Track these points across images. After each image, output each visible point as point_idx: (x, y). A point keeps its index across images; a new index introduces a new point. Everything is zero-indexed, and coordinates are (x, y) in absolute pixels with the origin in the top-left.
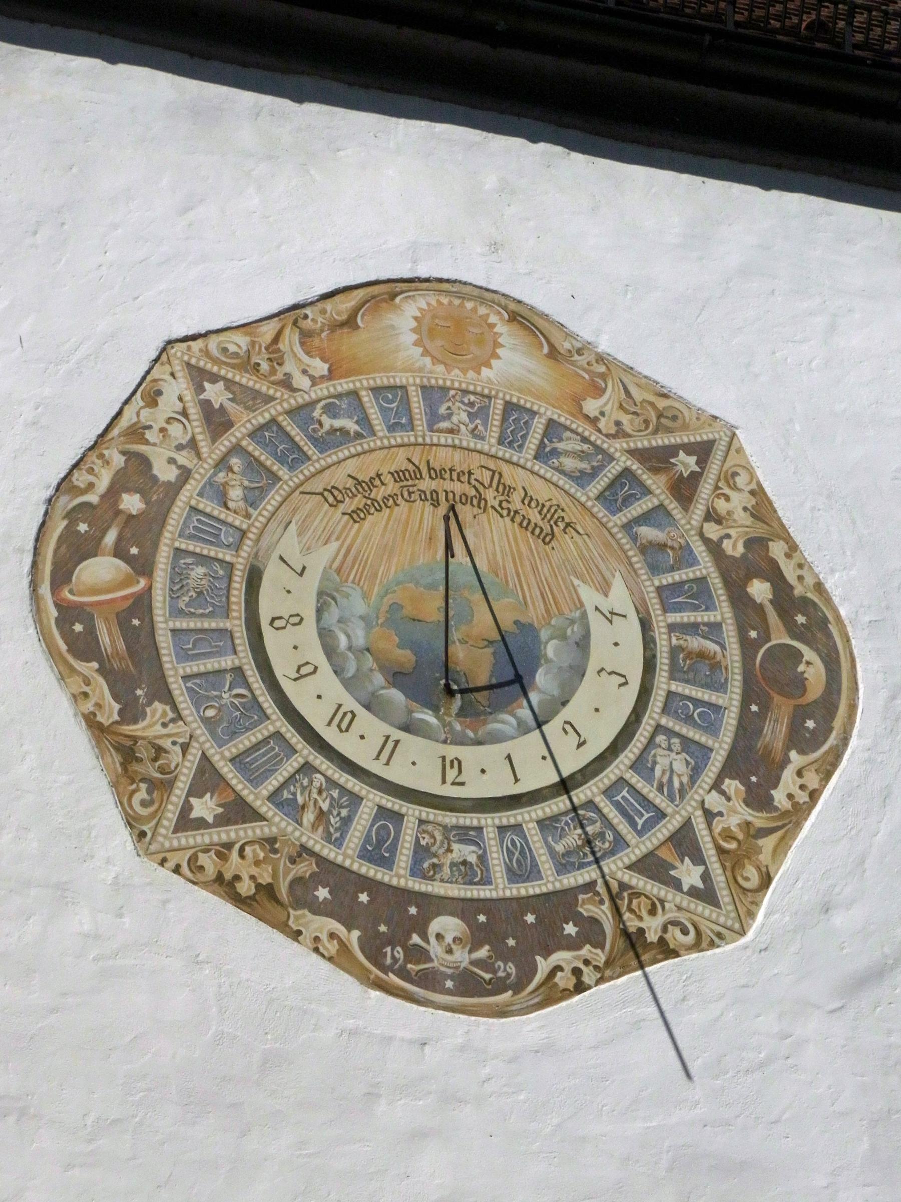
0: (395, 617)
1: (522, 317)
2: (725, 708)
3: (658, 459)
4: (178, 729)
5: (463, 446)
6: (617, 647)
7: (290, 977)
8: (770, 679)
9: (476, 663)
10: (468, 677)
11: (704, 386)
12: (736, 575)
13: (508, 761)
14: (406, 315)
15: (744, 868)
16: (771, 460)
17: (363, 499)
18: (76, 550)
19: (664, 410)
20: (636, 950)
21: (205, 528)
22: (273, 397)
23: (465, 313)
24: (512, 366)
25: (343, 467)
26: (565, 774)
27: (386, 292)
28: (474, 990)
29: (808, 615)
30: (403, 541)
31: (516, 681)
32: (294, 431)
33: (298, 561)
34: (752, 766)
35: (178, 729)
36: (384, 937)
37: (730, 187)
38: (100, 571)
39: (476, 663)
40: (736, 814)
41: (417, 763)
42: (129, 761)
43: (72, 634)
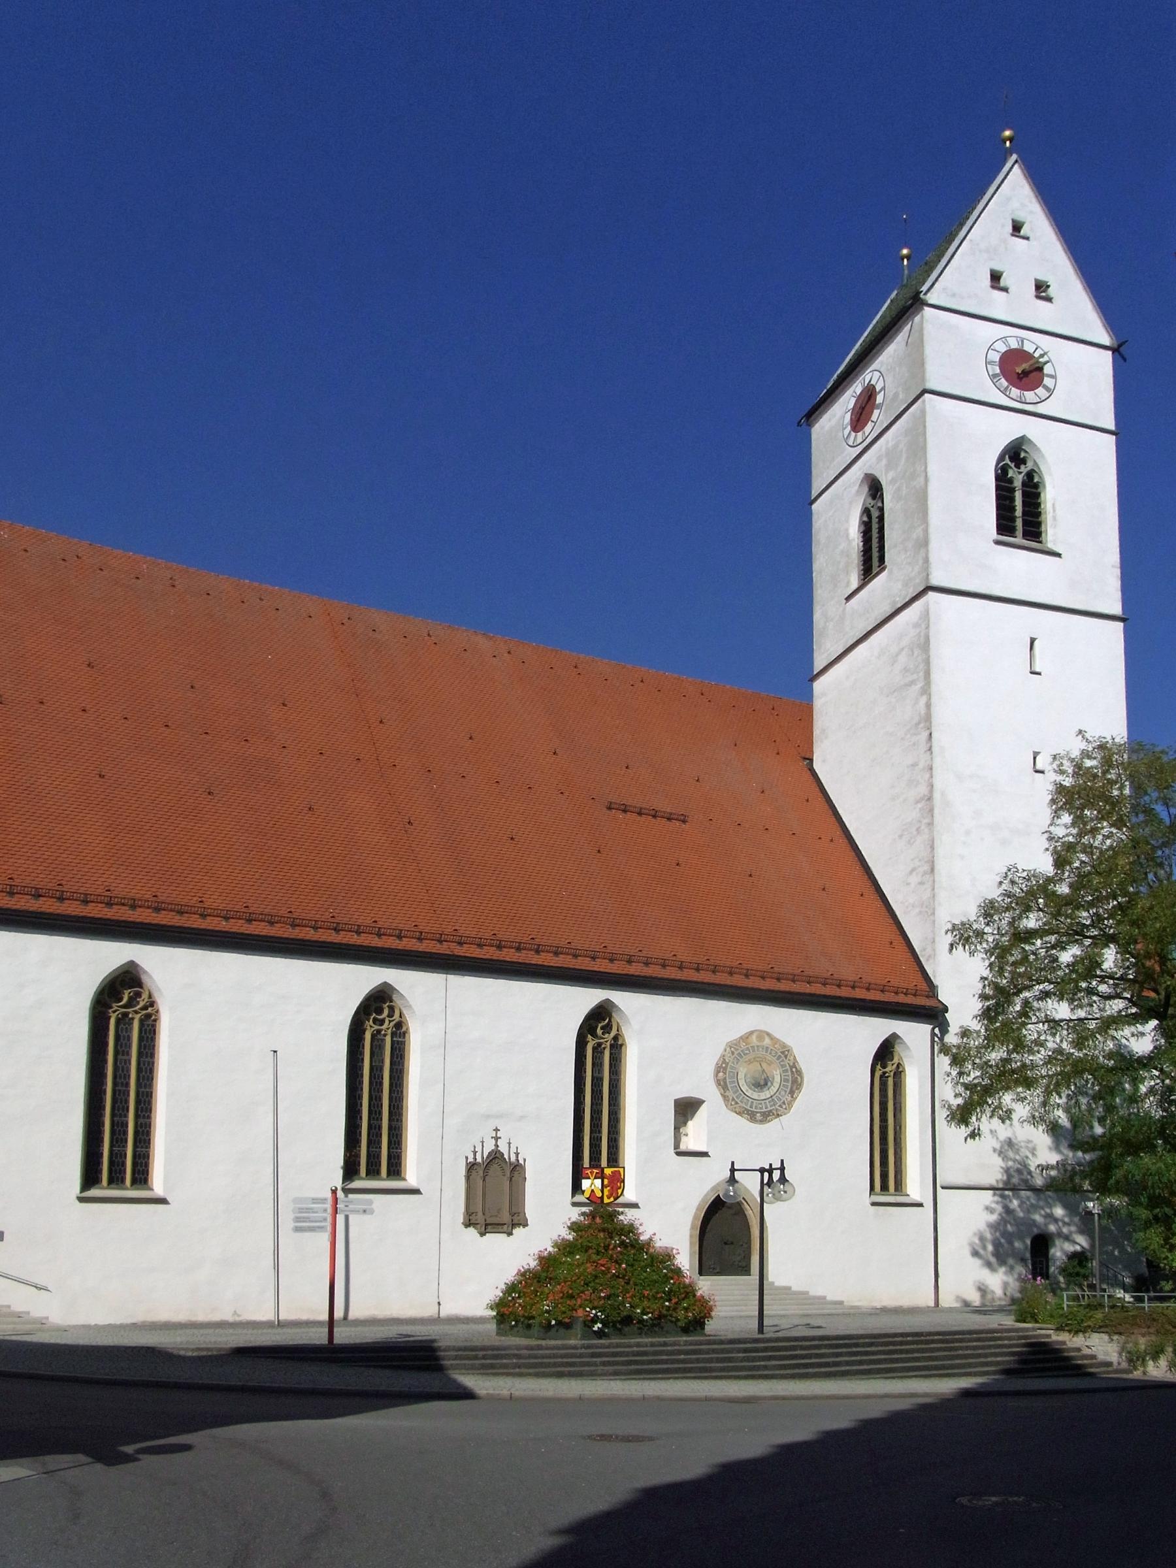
0: (754, 1078)
1: (768, 1034)
2: (732, 1180)
3: (783, 1053)
4: (730, 1094)
5: (762, 1053)
6: (777, 1079)
7: (742, 1122)
8: (795, 1081)
9: (762, 1083)
10: (761, 1084)
11: (789, 1042)
12: (791, 1068)
13: (766, 1094)
14: (754, 1037)
15: (790, 1105)
16: (796, 1052)
17: (750, 1062)
18: (718, 1072)
19: (784, 1045)
20: (778, 1116)
21: (732, 1068)
22: (740, 1049)
23: (762, 1034)
24: (767, 1041)
25: (747, 1058)
26: (1116, 609)
27: (752, 1033)
28: (761, 1122)
29: (799, 1072)
30: (755, 1067)
31: (766, 1084)
32: (1019, 523)
33: (742, 1071)
34: (792, 1092)
35: (730, 1094)
36: (752, 1116)
37: (235, 1313)
38: (721, 1074)
39: (762, 1083)
40: (789, 1098)
41: (755, 1096)
42: (725, 1097)
43: (718, 1083)
